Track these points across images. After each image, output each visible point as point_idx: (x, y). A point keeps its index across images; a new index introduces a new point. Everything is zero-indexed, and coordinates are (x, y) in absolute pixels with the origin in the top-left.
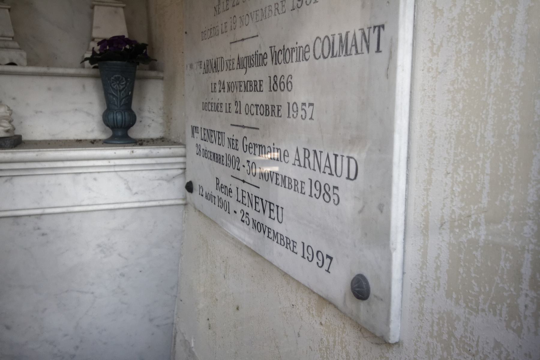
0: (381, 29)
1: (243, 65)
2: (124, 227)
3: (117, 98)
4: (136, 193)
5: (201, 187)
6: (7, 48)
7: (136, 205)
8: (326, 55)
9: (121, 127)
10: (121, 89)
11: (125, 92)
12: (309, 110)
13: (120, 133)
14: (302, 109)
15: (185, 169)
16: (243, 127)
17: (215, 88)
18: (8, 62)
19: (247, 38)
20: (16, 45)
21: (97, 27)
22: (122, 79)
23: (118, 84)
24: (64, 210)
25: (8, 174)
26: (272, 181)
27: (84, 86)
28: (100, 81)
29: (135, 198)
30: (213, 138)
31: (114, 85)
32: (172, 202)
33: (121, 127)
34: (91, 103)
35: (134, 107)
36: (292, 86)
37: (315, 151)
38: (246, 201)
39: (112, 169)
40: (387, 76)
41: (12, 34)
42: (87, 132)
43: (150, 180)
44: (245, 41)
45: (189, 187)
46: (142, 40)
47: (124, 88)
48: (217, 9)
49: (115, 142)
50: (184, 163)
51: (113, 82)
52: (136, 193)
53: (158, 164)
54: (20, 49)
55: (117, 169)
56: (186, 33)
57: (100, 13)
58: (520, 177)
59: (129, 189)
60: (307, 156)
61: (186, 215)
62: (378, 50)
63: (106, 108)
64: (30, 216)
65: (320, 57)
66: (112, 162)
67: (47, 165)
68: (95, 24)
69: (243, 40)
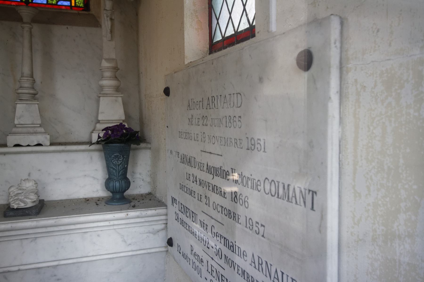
0: (314, 194)
1: (211, 172)
2: (120, 270)
3: (116, 170)
4: (130, 244)
5: (179, 246)
6: (36, 133)
7: (130, 253)
8: (273, 194)
9: (119, 192)
10: (119, 163)
11: (122, 165)
12: (261, 229)
13: (118, 196)
14: (256, 226)
15: (167, 224)
16: (211, 217)
17: (189, 177)
18: (36, 143)
19: (214, 154)
20: (42, 130)
21: (102, 113)
22: (120, 156)
23: (117, 160)
24: (75, 261)
25: (33, 236)
26: (234, 269)
27: (91, 158)
28: (103, 154)
29: (129, 248)
30: (188, 214)
31: (114, 161)
32: (157, 250)
33: (119, 192)
34: (96, 170)
35: (129, 176)
36: (248, 205)
37: (266, 263)
38: (214, 274)
39: (112, 228)
40: (320, 231)
41: (39, 122)
42: (94, 191)
43: (140, 234)
44: (212, 155)
45: (170, 242)
46: (136, 128)
47: (121, 163)
48: (191, 121)
49: (114, 204)
50: (167, 220)
51: (113, 159)
52: (130, 244)
53: (146, 222)
54: (45, 133)
55: (115, 227)
56: (167, 127)
57: (104, 102)
58: (421, 131)
59: (125, 241)
60: (260, 262)
61: (168, 259)
62: (312, 208)
63: (107, 177)
64: (48, 267)
65: (268, 193)
66: (112, 223)
67: (63, 228)
68: (100, 111)
69: (210, 153)
